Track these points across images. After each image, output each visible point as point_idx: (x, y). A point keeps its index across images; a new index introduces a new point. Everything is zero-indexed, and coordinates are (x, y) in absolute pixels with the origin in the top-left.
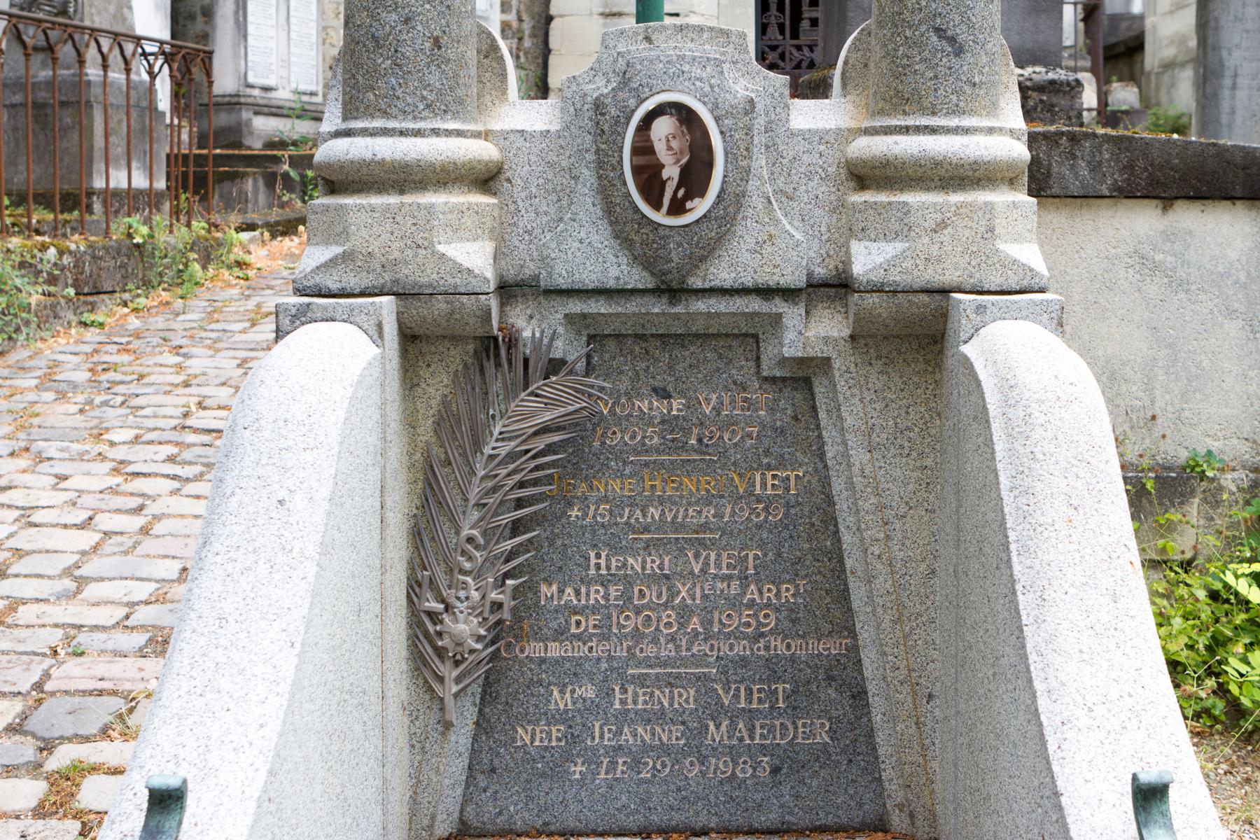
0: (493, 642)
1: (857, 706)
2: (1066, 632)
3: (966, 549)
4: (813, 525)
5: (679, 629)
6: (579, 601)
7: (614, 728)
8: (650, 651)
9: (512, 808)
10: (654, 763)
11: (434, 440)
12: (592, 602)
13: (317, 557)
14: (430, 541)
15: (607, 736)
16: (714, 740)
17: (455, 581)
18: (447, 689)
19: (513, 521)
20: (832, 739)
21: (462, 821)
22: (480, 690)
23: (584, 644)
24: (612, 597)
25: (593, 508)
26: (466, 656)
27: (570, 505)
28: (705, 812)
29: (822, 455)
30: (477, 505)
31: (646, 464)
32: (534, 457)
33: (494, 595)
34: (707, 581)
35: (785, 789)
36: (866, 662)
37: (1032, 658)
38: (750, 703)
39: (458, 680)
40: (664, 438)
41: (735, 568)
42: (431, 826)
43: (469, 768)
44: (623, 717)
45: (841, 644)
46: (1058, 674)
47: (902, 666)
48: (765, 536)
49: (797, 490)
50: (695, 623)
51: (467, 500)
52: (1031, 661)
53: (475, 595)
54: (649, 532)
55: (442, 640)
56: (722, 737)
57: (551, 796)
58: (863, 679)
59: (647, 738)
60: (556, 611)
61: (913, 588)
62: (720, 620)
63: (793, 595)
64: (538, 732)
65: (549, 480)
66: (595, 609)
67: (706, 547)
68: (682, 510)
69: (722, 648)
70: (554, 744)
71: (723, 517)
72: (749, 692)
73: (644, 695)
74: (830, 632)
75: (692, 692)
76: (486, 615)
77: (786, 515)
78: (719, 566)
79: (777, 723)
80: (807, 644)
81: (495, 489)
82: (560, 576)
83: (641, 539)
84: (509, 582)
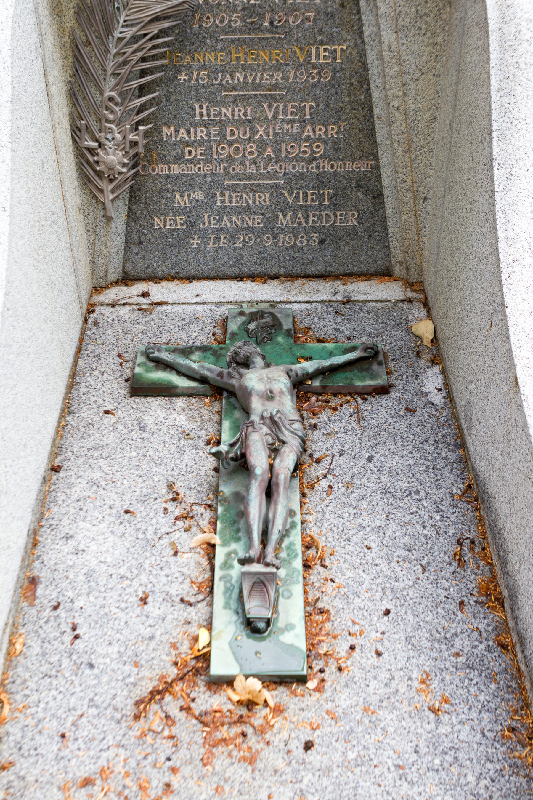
0: (134, 167)
1: (376, 203)
2: (524, 199)
3: (460, 115)
4: (352, 84)
5: (258, 155)
6: (190, 137)
7: (217, 217)
8: (239, 170)
9: (155, 264)
10: (244, 238)
11: (76, 26)
12: (198, 138)
13: (10, 145)
14: (83, 100)
15: (213, 222)
16: (282, 224)
17: (103, 127)
18: (106, 197)
19: (140, 86)
20: (359, 223)
21: (124, 272)
22: (128, 195)
23: (195, 166)
24: (212, 135)
25: (195, 73)
26: (117, 176)
27: (179, 72)
28: (277, 266)
29: (361, 34)
30: (113, 74)
31: (233, 41)
32: (151, 39)
33: (131, 137)
34: (277, 123)
35: (328, 252)
36: (384, 176)
37: (499, 214)
38: (306, 201)
39: (113, 191)
40: (245, 21)
41: (296, 115)
42: (106, 276)
43: (126, 242)
44: (223, 211)
45: (368, 164)
46: (515, 227)
47: (408, 180)
48: (318, 92)
49: (342, 59)
50: (269, 152)
51: (105, 70)
52: (497, 217)
53: (118, 137)
54: (236, 90)
55: (99, 166)
56: (287, 222)
57: (179, 257)
58: (381, 187)
59: (239, 223)
60: (175, 145)
61: (419, 129)
62: (286, 150)
63: (337, 133)
64: (168, 220)
65: (163, 56)
66: (201, 143)
67: (276, 101)
68: (259, 75)
69: (288, 168)
70: (179, 227)
71: (288, 79)
72: (306, 195)
73: (236, 197)
74: (361, 157)
75: (268, 195)
76: (127, 150)
77: (333, 78)
78: (285, 113)
79: (324, 214)
80: (345, 164)
81: (125, 63)
82: (176, 121)
83: (230, 95)
84: (141, 128)
